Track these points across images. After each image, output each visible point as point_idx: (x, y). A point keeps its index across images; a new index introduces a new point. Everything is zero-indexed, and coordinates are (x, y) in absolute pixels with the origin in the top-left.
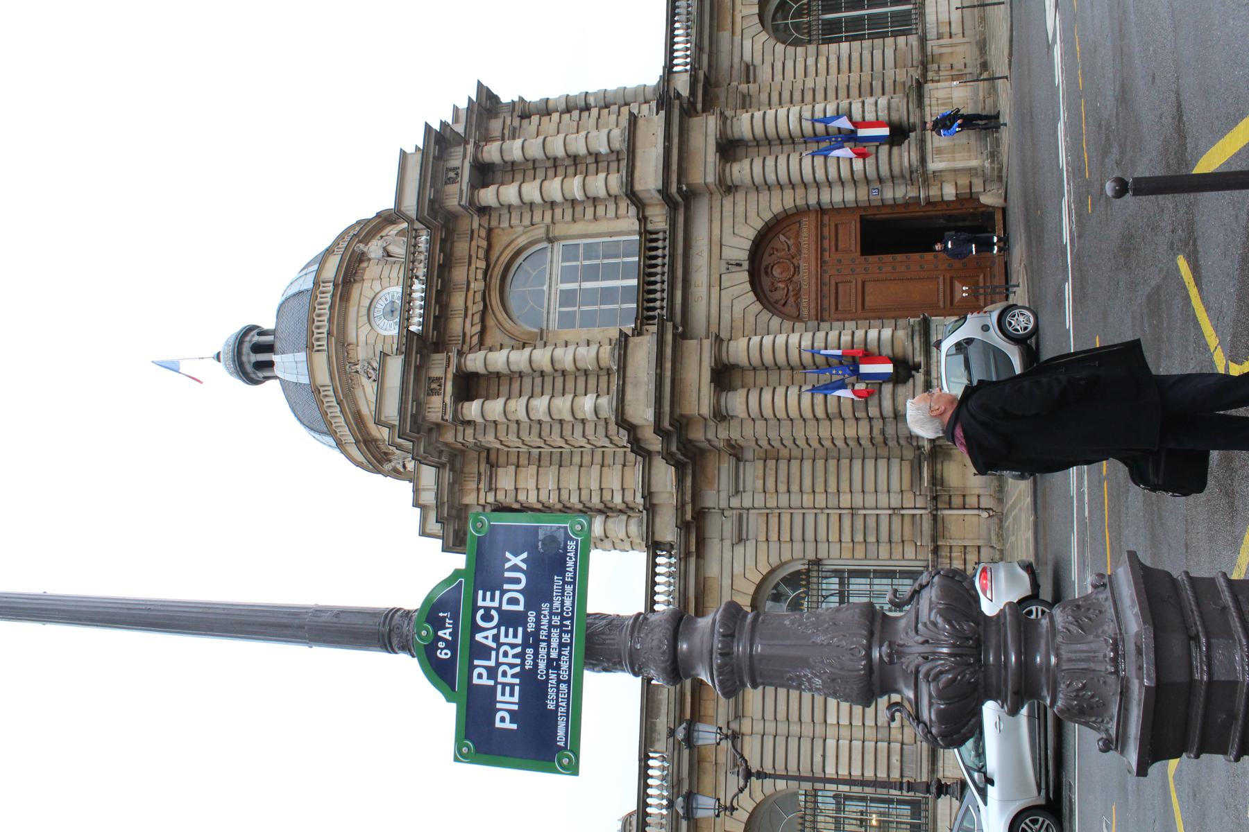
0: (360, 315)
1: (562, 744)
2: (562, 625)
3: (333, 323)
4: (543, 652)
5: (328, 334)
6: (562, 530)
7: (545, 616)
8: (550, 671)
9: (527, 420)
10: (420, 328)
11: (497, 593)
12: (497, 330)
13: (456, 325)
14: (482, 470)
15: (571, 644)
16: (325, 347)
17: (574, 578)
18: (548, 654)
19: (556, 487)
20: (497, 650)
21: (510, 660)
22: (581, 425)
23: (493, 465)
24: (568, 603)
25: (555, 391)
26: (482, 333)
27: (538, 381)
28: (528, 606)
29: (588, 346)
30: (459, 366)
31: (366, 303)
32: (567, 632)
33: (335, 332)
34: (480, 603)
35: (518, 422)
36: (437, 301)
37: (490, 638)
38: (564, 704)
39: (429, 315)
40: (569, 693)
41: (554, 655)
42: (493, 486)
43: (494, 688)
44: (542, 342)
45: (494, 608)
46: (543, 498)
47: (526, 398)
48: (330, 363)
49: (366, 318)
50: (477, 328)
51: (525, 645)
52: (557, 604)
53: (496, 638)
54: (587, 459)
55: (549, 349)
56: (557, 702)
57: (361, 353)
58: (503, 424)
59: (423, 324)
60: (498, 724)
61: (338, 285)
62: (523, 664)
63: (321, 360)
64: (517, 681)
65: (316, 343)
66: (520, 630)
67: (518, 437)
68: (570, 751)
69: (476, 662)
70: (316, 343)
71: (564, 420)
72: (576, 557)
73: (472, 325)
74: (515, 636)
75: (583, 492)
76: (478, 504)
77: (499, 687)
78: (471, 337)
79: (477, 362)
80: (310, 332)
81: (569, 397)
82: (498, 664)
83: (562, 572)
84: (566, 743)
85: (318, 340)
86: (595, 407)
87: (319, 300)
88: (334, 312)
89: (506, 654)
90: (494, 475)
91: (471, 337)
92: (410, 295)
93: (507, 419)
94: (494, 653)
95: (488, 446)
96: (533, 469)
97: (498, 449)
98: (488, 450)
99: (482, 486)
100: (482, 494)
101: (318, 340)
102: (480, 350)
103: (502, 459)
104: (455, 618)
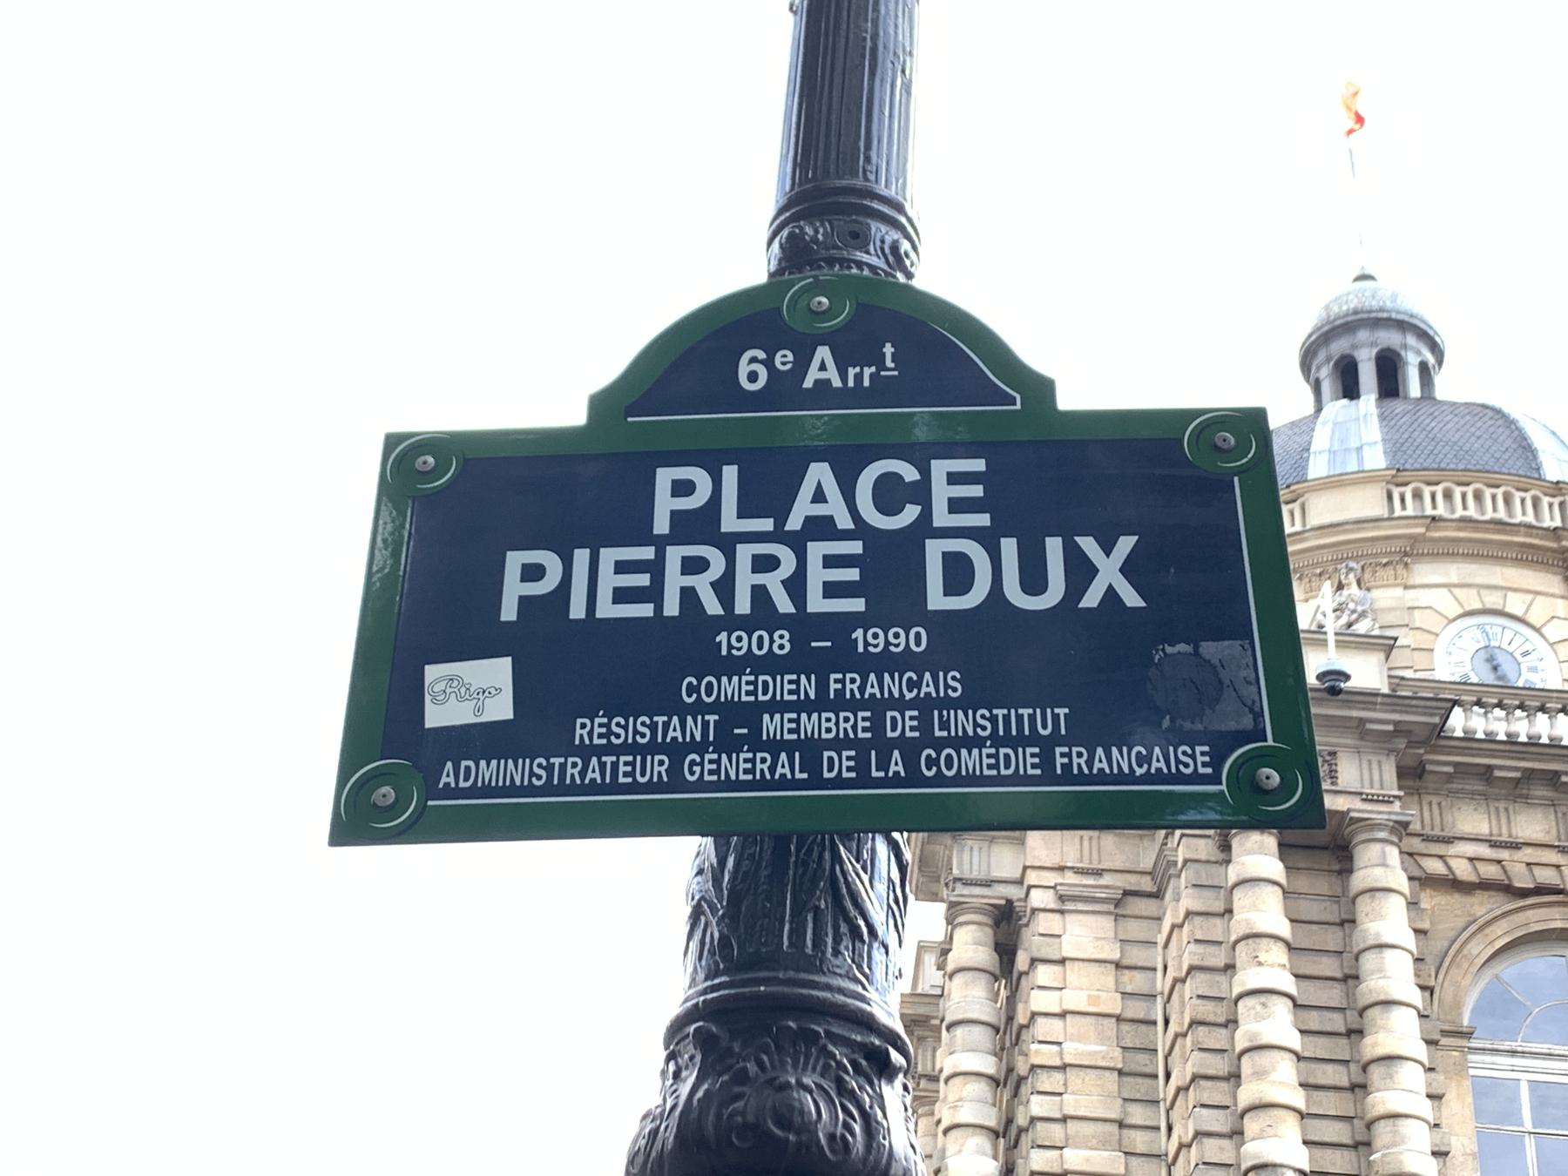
0: (1483, 592)
1: (447, 779)
2: (884, 748)
3: (1459, 529)
4: (783, 687)
5: (1434, 519)
6: (1247, 722)
7: (912, 685)
8: (712, 718)
9: (1236, 991)
10: (1459, 733)
11: (983, 520)
12: (1460, 923)
13: (1472, 820)
14: (1106, 880)
15: (816, 781)
16: (1398, 512)
17: (1068, 777)
18: (776, 707)
19: (1068, 1059)
20: (778, 536)
21: (745, 580)
22: (1225, 1129)
23: (1120, 904)
24: (970, 760)
25: (1313, 1066)
26: (1455, 885)
27: (1337, 1022)
28: (941, 623)
29: (1434, 1154)
30: (1368, 825)
31: (1515, 604)
32: (862, 766)
33: (1437, 534)
34: (940, 468)
35: (1230, 968)
36: (1529, 775)
37: (819, 510)
38: (593, 775)
39: (1492, 754)
40: (634, 788)
41: (771, 725)
42: (1069, 906)
43: (643, 536)
44: (1436, 1036)
45: (927, 513)
46: (1043, 1028)
47: (1293, 990)
48: (1360, 523)
49: (1477, 606)
50: (1463, 870)
51: (803, 625)
52: (962, 722)
53: (821, 528)
54: (1140, 1141)
55: (1421, 1051)
56: (600, 751)
57: (1386, 597)
58: (1228, 931)
59: (1469, 737)
60: (515, 561)
61: (1558, 539)
62: (730, 621)
63: (1367, 503)
64: (672, 608)
65: (1408, 491)
66: (857, 605)
67: (1192, 969)
68: (422, 809)
69: (730, 473)
70: (1408, 491)
71: (1238, 1085)
72: (1148, 779)
73: (1471, 859)
74: (831, 590)
75: (1057, 1127)
76: (1025, 868)
77: (648, 553)
78: (1441, 857)
79: (1378, 871)
80: (1432, 475)
81: (1298, 1099)
82: (728, 545)
83: (1086, 732)
84: (449, 793)
85: (1417, 495)
86: (1275, 1166)
87: (1518, 495)
88: (1486, 531)
89: (765, 564)
90: (1097, 907)
91: (1441, 857)
92: (1542, 709)
93: (1237, 942)
94: (766, 525)
95: (1169, 895)
96: (1113, 1004)
97: (1159, 919)
98: (1157, 895)
99: (1070, 878)
100: (1051, 878)
101: (1417, 495)
102: (1411, 879)
103: (1134, 929)
104: (881, 392)
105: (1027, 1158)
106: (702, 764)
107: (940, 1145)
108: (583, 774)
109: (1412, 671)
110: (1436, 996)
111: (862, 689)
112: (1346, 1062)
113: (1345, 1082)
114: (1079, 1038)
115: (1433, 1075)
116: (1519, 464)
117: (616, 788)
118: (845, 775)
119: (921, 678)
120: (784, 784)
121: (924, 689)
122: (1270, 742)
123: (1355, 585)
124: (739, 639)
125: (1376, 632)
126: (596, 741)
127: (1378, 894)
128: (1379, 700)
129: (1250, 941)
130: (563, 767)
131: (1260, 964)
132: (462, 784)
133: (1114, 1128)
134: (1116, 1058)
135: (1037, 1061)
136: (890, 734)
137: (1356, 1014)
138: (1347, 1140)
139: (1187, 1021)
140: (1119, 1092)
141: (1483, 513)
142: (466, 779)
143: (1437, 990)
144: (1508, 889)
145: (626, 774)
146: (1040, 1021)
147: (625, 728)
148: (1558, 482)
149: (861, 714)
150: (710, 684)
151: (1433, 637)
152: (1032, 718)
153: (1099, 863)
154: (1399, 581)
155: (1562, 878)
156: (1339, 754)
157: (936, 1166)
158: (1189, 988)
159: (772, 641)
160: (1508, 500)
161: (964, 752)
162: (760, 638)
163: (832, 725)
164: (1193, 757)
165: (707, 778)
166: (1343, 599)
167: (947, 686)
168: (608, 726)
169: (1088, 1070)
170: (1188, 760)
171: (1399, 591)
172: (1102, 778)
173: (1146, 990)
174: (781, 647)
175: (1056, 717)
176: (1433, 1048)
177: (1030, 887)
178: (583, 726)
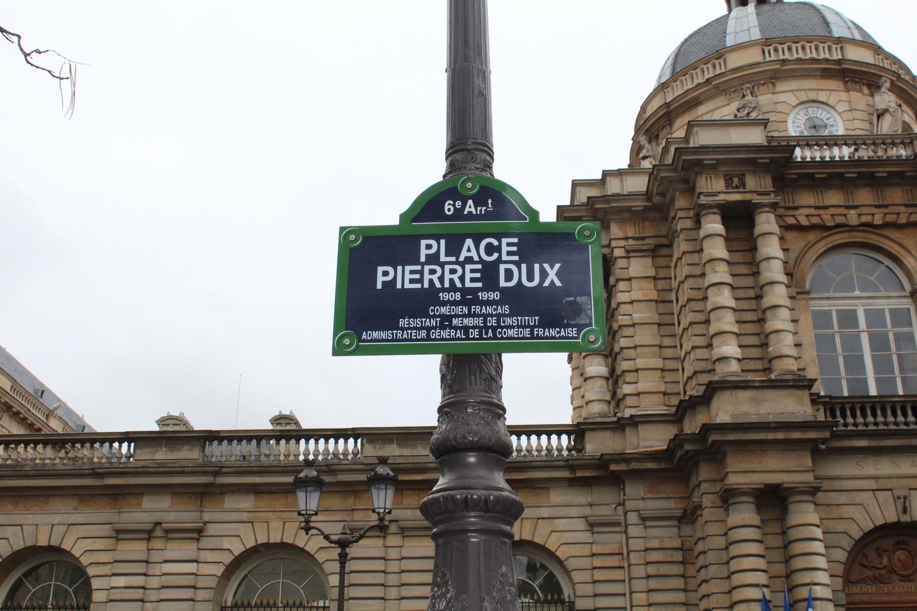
1: (364, 337)
2: (487, 328)
4: (459, 310)
6: (588, 321)
7: (495, 310)
8: (438, 319)
9: (706, 284)
10: (799, 159)
13: (806, 199)
14: (648, 241)
15: (468, 338)
16: (768, 59)
17: (538, 337)
18: (457, 316)
19: (635, 321)
21: (447, 276)
24: (511, 332)
26: (799, 228)
27: (751, 293)
30: (760, 205)
31: (822, 97)
32: (480, 334)
35: (703, 275)
38: (405, 336)
40: (417, 340)
41: (455, 322)
43: (416, 262)
44: (795, 295)
46: (624, 309)
48: (751, 66)
49: (805, 99)
50: (804, 222)
51: (464, 291)
52: (509, 321)
53: (469, 260)
54: (669, 353)
57: (765, 99)
58: (700, 259)
60: (380, 269)
61: (840, 65)
62: (443, 290)
64: (426, 285)
66: (479, 285)
67: (687, 277)
68: (358, 346)
69: (443, 242)
71: (709, 324)
72: (560, 338)
73: (807, 216)
76: (611, 240)
77: (418, 268)
81: (735, 328)
82: (442, 265)
83: (544, 324)
84: (365, 341)
85: (776, 50)
87: (821, 45)
88: (808, 64)
89: (453, 271)
92: (836, 145)
94: (453, 259)
97: (671, 256)
99: (631, 242)
100: (622, 243)
101: (776, 50)
102: (780, 227)
103: (661, 261)
105: (620, 365)
106: (435, 333)
107: (582, 364)
108: (402, 336)
109: (777, 132)
110: (794, 277)
111: (481, 311)
112: (755, 310)
113: (755, 319)
114: (639, 312)
115: (793, 312)
116: (821, 30)
117: (411, 340)
118: (476, 336)
119: (498, 307)
120: (459, 339)
121: (498, 311)
122: (593, 327)
123: (750, 95)
124: (446, 295)
125: (760, 117)
126: (406, 326)
127: (766, 236)
128: (762, 148)
129: (711, 262)
130: (396, 333)
131: (716, 272)
132: (368, 338)
133: (657, 349)
134: (656, 318)
135: (622, 323)
136: (488, 325)
137: (759, 289)
138: (758, 343)
139: (686, 300)
140: (659, 333)
141: (806, 55)
142: (370, 337)
143: (794, 274)
144: (822, 227)
145: (414, 336)
146: (622, 306)
147: (414, 322)
148: (839, 37)
149: (480, 319)
150: (437, 309)
151: (786, 115)
152: (528, 320)
153: (643, 233)
154: (770, 91)
155: (847, 220)
156: (746, 175)
157: (581, 372)
158: (686, 285)
159: (455, 296)
160: (817, 48)
161: (509, 330)
162: (452, 295)
163: (472, 322)
164: (572, 332)
165: (437, 337)
166: (745, 102)
167: (505, 310)
168: (409, 321)
169: (644, 325)
170: (571, 333)
171: (770, 96)
172: (547, 338)
173: (667, 288)
174: (458, 298)
175: (535, 320)
176: (793, 300)
177: (613, 248)
178: (402, 321)
